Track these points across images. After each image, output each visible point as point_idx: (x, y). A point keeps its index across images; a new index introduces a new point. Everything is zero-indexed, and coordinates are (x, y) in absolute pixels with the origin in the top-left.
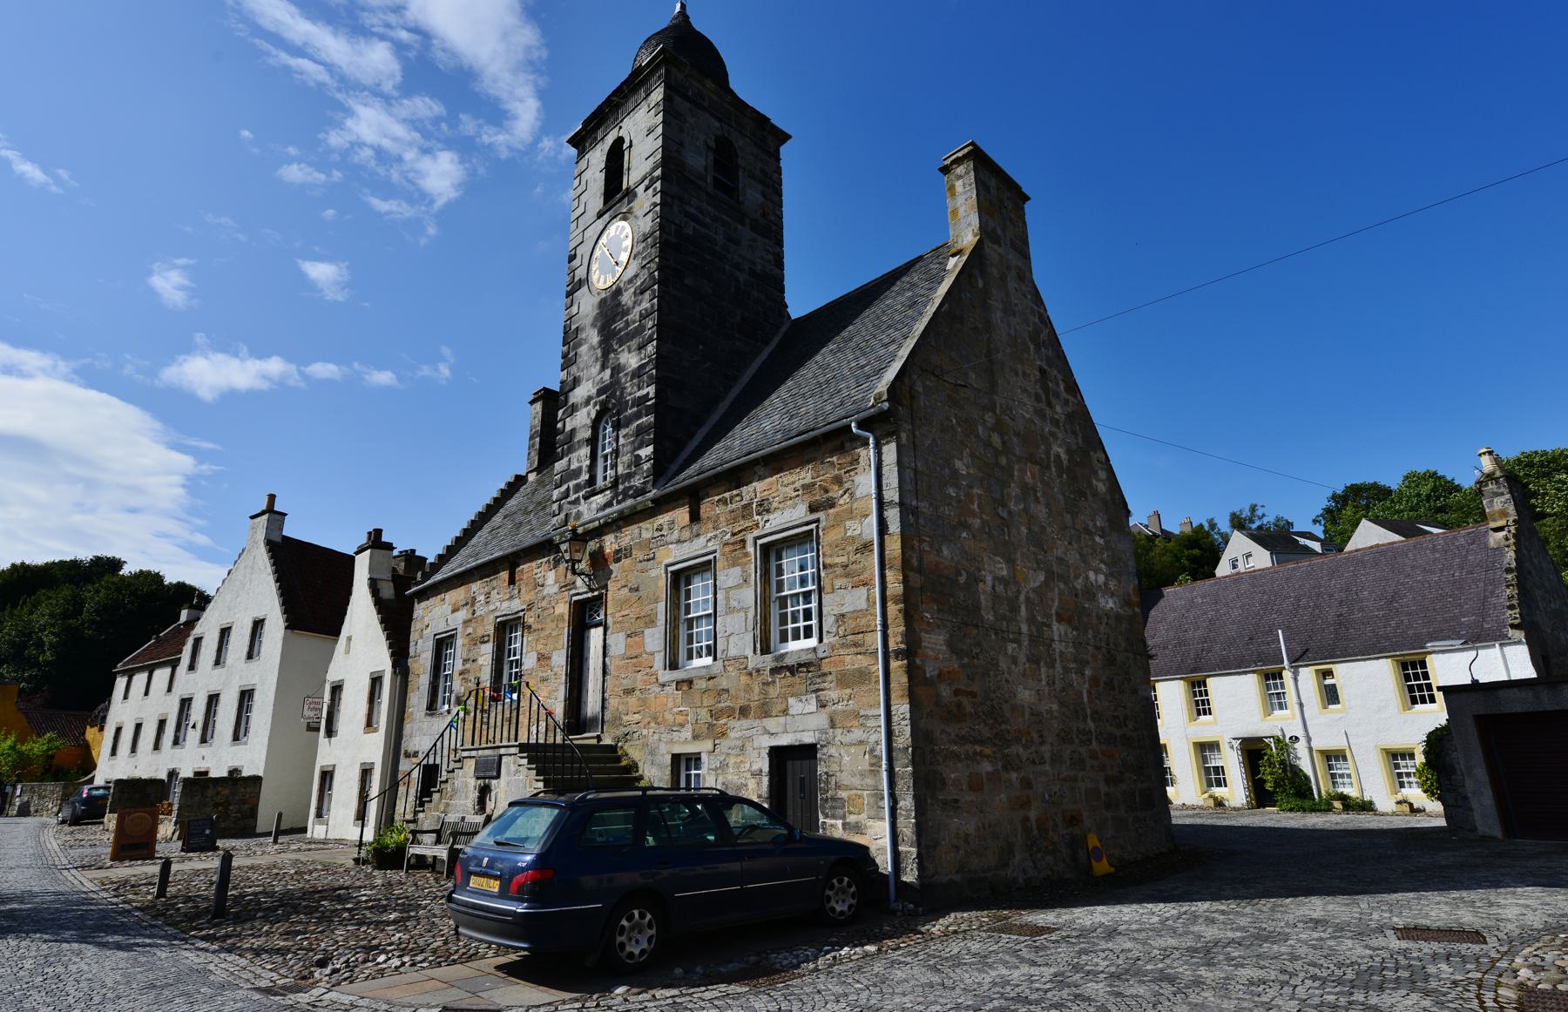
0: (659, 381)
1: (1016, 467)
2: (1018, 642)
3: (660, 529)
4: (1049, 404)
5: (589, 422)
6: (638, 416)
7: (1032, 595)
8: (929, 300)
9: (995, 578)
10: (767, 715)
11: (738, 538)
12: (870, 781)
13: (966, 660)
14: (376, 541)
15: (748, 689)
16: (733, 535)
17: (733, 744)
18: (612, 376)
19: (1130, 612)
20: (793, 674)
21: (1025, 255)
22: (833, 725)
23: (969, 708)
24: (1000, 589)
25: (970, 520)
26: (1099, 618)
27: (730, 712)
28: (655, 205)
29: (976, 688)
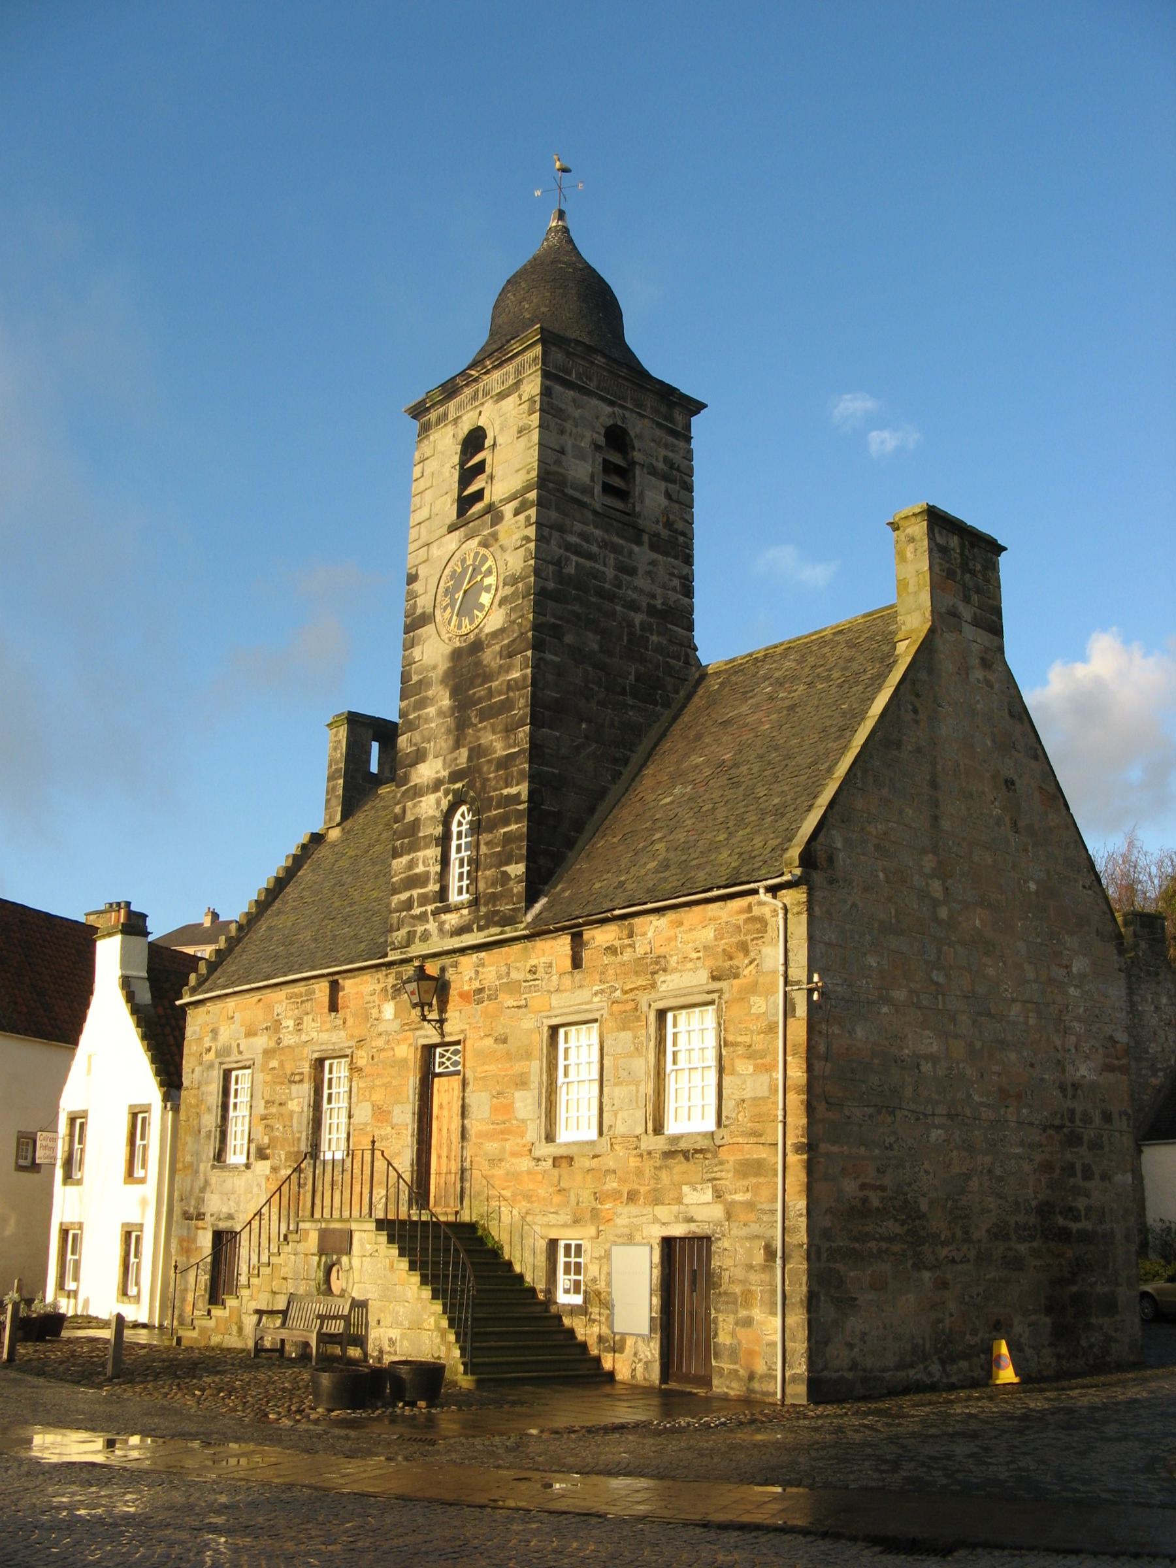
0: (533, 778)
3: (533, 971)
5: (438, 814)
6: (505, 820)
8: (862, 716)
10: (657, 1201)
11: (630, 996)
12: (765, 1277)
14: (134, 925)
15: (639, 1172)
17: (619, 1232)
18: (470, 759)
20: (687, 1159)
21: (996, 630)
23: (875, 1202)
27: (615, 1195)
28: (527, 539)
29: (887, 1181)
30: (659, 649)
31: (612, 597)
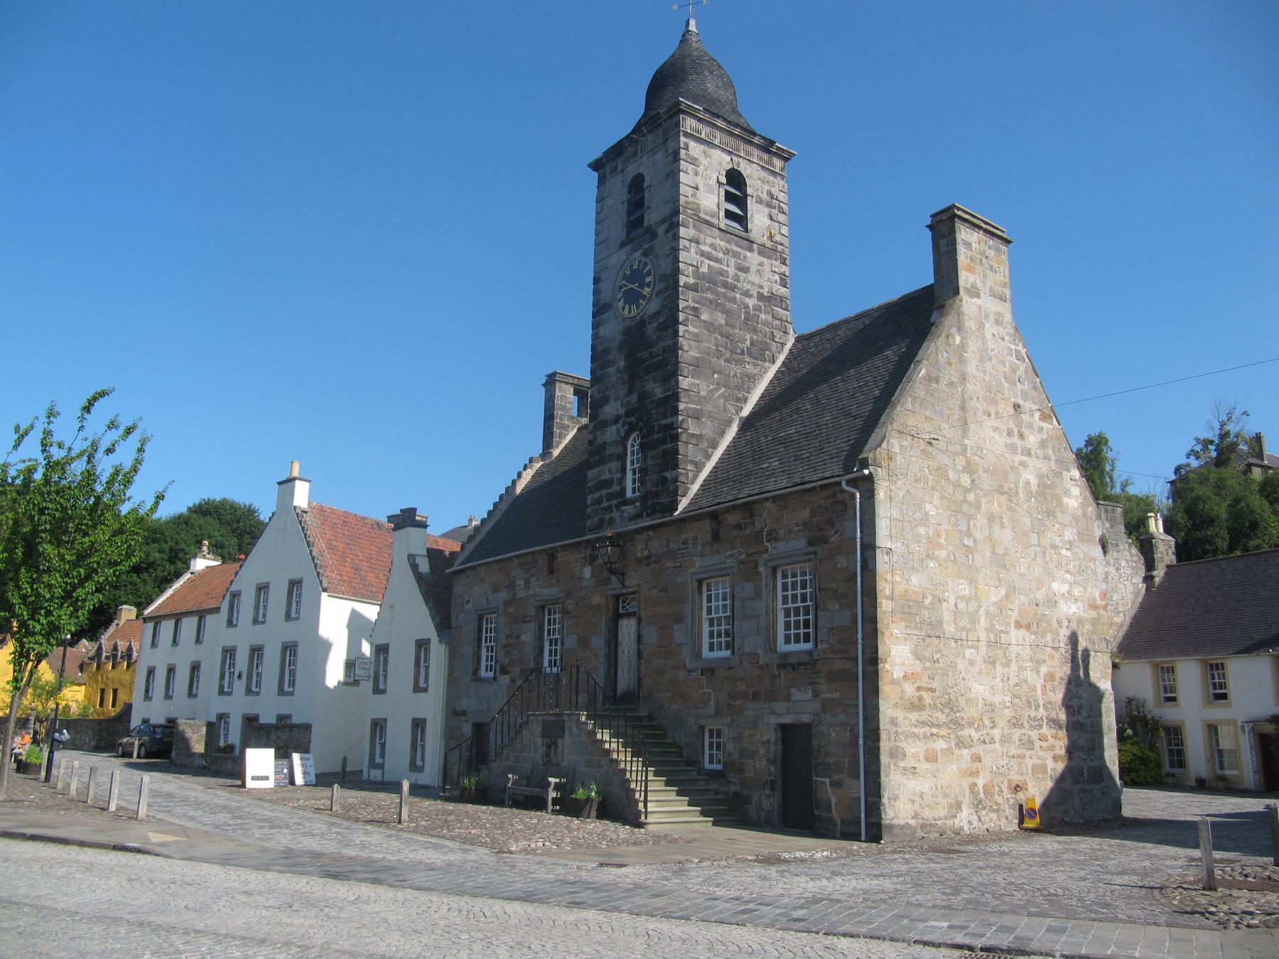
1: (984, 500)
2: (976, 648)
3: (685, 542)
4: (1021, 436)
7: (992, 609)
9: (958, 597)
13: (928, 664)
16: (748, 555)
18: (639, 400)
19: (1094, 614)
22: (824, 710)
24: (962, 606)
25: (937, 553)
26: (1059, 622)
29: (935, 685)
30: (766, 323)
31: (733, 288)
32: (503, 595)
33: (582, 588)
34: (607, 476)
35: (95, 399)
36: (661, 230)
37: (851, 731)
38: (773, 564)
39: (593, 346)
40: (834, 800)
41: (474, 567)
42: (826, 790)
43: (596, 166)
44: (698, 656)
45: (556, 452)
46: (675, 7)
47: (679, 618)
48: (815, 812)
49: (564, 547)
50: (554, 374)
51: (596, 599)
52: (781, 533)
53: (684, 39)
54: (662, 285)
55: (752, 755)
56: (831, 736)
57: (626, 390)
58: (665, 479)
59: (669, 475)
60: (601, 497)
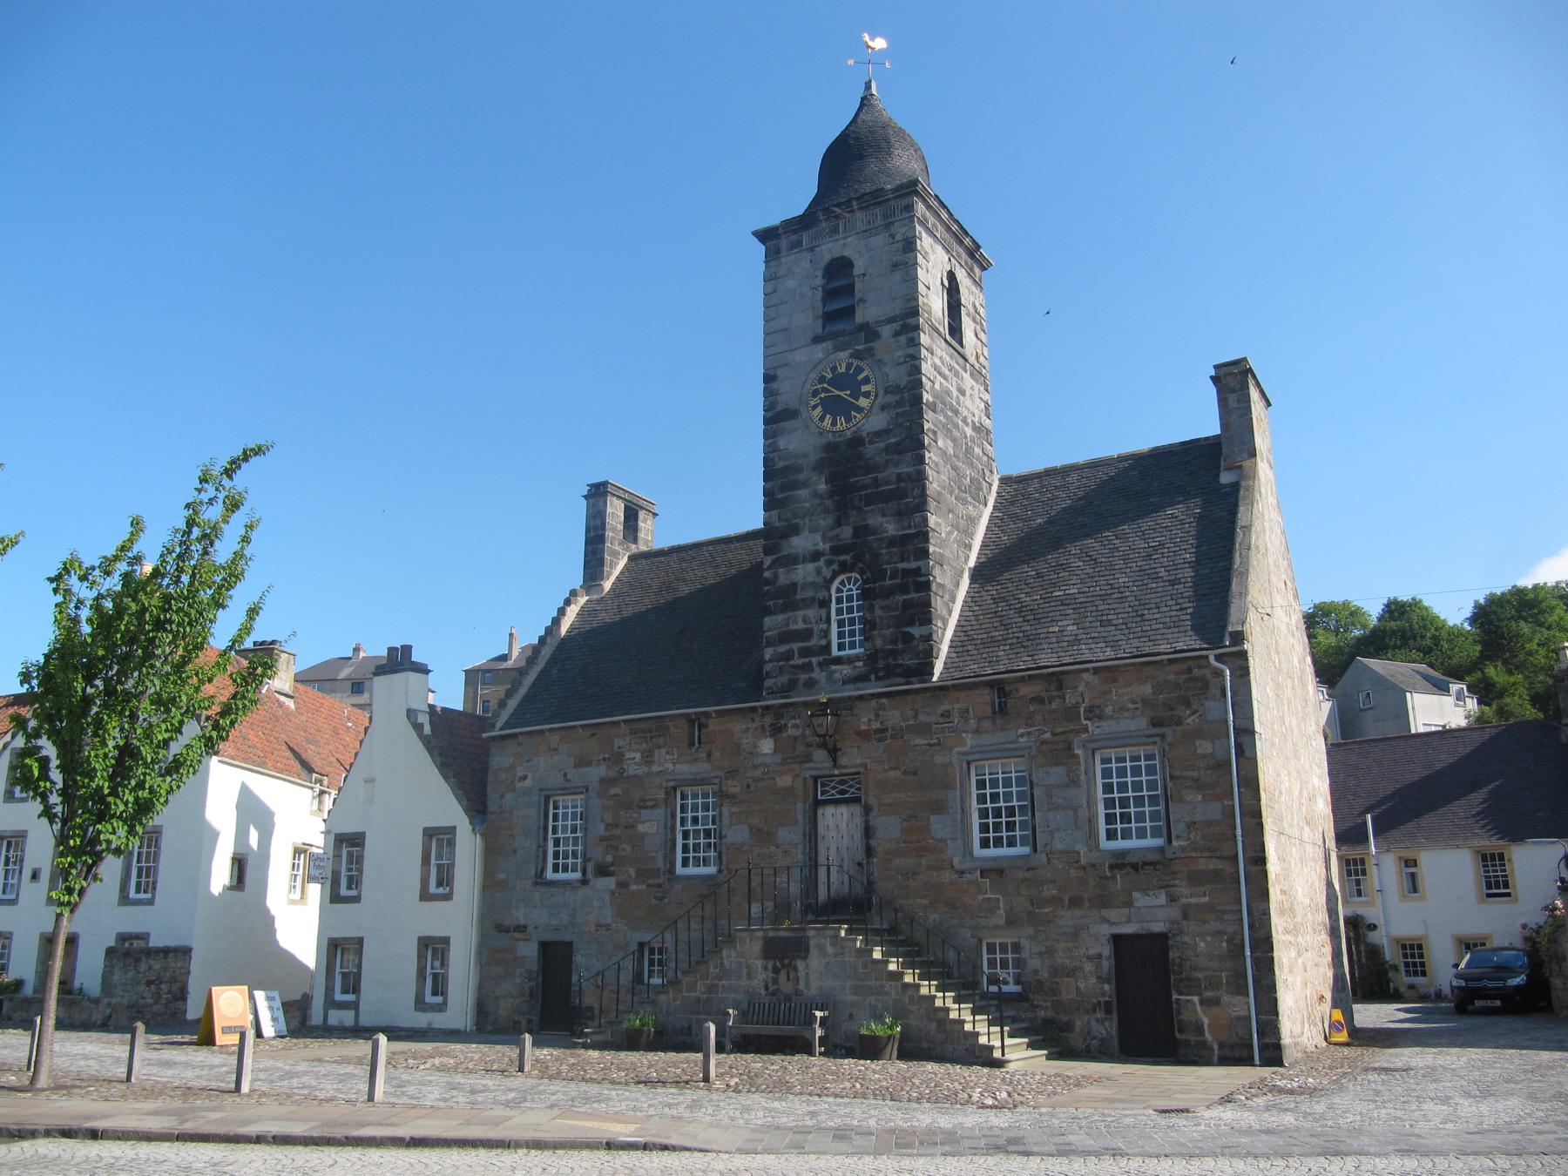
16: (1055, 735)
22: (1185, 916)
32: (596, 772)
33: (755, 767)
34: (800, 625)
35: (246, 457)
36: (886, 331)
37: (1229, 941)
38: (1093, 745)
39: (767, 462)
40: (1206, 1021)
41: (541, 732)
42: (1193, 1007)
43: (764, 235)
44: (968, 852)
45: (607, 585)
46: (851, 62)
47: (940, 808)
48: (1178, 1036)
49: (720, 714)
50: (605, 484)
51: (785, 781)
52: (1109, 710)
53: (866, 101)
54: (891, 399)
55: (1072, 972)
56: (1200, 947)
57: (830, 520)
58: (908, 638)
59: (916, 631)
60: (790, 652)
